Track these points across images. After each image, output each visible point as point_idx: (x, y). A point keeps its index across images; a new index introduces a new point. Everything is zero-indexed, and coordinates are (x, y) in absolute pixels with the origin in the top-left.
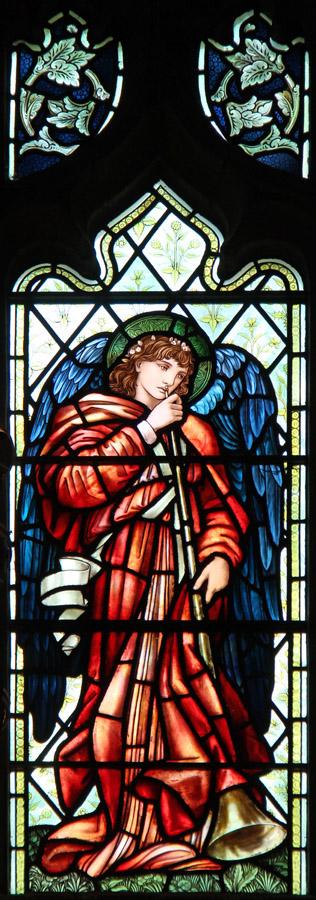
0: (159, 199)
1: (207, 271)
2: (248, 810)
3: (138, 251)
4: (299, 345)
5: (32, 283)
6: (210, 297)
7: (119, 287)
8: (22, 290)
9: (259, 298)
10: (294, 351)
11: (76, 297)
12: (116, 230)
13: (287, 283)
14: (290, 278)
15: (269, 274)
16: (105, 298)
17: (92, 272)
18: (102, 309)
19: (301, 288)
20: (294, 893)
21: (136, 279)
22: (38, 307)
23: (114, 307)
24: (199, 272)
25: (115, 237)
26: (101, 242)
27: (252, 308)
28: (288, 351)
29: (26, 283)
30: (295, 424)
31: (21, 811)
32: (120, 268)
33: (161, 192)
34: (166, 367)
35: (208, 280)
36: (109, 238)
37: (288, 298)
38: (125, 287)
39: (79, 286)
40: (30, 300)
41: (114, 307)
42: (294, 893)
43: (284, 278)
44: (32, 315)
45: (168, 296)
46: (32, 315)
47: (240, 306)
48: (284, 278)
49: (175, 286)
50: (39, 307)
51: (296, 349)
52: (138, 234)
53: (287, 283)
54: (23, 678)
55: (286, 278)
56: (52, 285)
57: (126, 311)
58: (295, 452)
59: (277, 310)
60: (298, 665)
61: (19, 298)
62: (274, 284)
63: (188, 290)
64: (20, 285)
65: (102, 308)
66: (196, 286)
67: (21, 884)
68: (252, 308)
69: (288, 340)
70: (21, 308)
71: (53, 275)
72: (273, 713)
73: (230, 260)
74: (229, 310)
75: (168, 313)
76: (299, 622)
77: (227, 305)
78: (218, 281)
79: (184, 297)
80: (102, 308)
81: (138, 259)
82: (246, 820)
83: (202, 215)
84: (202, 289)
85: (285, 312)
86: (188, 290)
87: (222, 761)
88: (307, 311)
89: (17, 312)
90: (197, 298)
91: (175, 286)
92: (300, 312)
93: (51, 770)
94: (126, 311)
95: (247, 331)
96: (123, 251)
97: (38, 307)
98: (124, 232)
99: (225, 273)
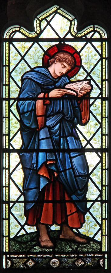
1: (72, 30)
3: (49, 23)
5: (11, 34)
6: (76, 39)
7: (43, 36)
8: (8, 37)
9: (90, 40)
11: (28, 40)
13: (100, 35)
15: (95, 31)
16: (37, 40)
17: (31, 29)
18: (36, 44)
20: (8, 43)
21: (48, 34)
22: (14, 43)
24: (70, 32)
25: (41, 21)
26: (36, 23)
28: (101, 59)
29: (9, 34)
31: (7, 123)
34: (65, 67)
35: (73, 33)
37: (101, 40)
39: (27, 34)
40: (11, 41)
42: (8, 43)
43: (99, 33)
44: (11, 45)
45: (59, 39)
46: (11, 45)
47: (32, 43)
48: (99, 33)
49: (62, 36)
50: (14, 43)
51: (104, 56)
52: (49, 19)
53: (100, 35)
54: (7, 153)
56: (18, 36)
59: (97, 44)
60: (105, 79)
61: (6, 40)
62: (97, 36)
63: (66, 38)
64: (6, 36)
65: (89, 43)
66: (69, 36)
67: (7, 248)
71: (19, 31)
76: (6, 42)
78: (76, 31)
79: (65, 39)
80: (89, 43)
84: (72, 37)
85: (100, 45)
86: (66, 38)
87: (62, 170)
88: (108, 44)
89: (6, 45)
91: (62, 36)
92: (105, 44)
93: (11, 200)
95: (87, 50)
97: (14, 43)
98: (45, 18)
99: (80, 29)
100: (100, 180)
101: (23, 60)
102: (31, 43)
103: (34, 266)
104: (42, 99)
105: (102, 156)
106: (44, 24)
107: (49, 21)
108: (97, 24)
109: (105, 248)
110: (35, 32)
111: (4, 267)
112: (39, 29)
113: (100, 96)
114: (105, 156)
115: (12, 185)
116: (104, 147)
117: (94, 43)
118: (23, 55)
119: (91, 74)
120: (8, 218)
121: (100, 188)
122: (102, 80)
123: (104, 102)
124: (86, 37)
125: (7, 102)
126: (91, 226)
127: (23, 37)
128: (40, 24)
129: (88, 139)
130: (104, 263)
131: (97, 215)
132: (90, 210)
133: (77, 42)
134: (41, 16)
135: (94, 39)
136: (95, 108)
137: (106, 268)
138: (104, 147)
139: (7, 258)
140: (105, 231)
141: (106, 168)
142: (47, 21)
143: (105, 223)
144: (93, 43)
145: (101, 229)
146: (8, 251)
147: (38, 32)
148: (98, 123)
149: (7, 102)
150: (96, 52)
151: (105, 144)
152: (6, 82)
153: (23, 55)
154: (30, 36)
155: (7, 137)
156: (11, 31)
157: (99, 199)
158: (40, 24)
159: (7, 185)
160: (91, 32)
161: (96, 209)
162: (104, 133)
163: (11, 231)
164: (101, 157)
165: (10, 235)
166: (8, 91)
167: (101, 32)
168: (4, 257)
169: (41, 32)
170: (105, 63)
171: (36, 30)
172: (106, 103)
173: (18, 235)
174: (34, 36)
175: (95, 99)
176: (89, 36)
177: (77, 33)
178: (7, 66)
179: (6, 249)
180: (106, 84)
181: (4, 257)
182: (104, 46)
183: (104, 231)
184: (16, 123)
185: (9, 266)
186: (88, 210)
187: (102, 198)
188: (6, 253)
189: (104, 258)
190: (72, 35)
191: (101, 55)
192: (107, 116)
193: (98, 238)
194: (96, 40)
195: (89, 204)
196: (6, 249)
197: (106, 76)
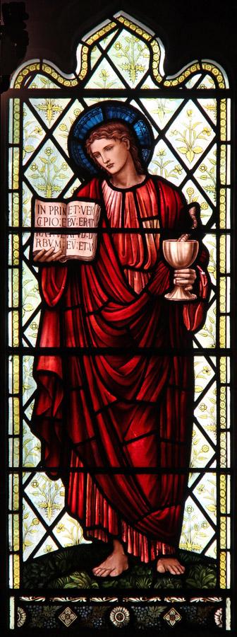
0: (120, 27)
2: (135, 175)
3: (104, 54)
4: (226, 134)
6: (163, 92)
8: (18, 86)
9: (196, 94)
10: (77, 83)
11: (62, 92)
12: (90, 42)
13: (216, 83)
14: (219, 78)
16: (78, 92)
17: (68, 65)
19: (228, 87)
21: (103, 79)
22: (31, 100)
23: (200, 100)
24: (150, 72)
25: (91, 48)
27: (190, 102)
28: (217, 140)
29: (21, 79)
30: (222, 200)
32: (149, 77)
33: (121, 20)
36: (86, 50)
37: (217, 94)
38: (98, 84)
39: (61, 80)
40: (26, 94)
41: (200, 100)
44: (25, 106)
46: (25, 106)
48: (214, 78)
50: (34, 101)
51: (223, 138)
52: (104, 44)
55: (212, 76)
56: (39, 82)
57: (90, 102)
58: (222, 226)
59: (209, 103)
60: (224, 548)
61: (15, 94)
62: (208, 83)
63: (142, 88)
64: (15, 83)
65: (77, 101)
66: (149, 84)
67: (17, 581)
68: (190, 102)
69: (217, 129)
70: (17, 101)
72: (195, 426)
73: (172, 66)
74: (174, 104)
75: (89, 603)
77: (168, 100)
79: (139, 93)
80: (77, 101)
81: (105, 59)
82: (136, 179)
83: (8, 390)
90: (150, 94)
91: (133, 86)
92: (227, 105)
93: (26, 465)
94: (90, 102)
96: (96, 54)
97: (31, 100)
98: (96, 43)
99: (171, 68)
100: (214, 502)
101: (49, 127)
102: (68, 100)
103: (74, 624)
104: (95, 232)
105: (220, 455)
106: (96, 54)
107: (104, 48)
108: (204, 58)
109: (226, 582)
110: (75, 74)
111: (12, 626)
112: (85, 65)
113: (214, 227)
114: (225, 362)
115: (27, 509)
116: (222, 346)
117: (203, 102)
118: (49, 128)
119: (194, 175)
120: (17, 188)
121: (215, 521)
122: (219, 186)
123: (222, 478)
124: (185, 88)
125: (16, 238)
126: (197, 135)
127: (52, 86)
128: (89, 55)
129: (190, 167)
130: (224, 618)
131: (209, 503)
132: (194, 175)
133: (163, 100)
134: (90, 38)
135: (200, 90)
136: (202, 174)
137: (228, 628)
138: (222, 346)
139: (19, 603)
140: (226, 540)
141: (226, 586)
142: (100, 48)
143: (226, 524)
144: (201, 101)
145: (217, 537)
146: (18, 588)
147: (84, 73)
148: (210, 368)
149: (16, 238)
150: (204, 519)
151: (225, 541)
152: (13, 261)
153: (49, 128)
154: (67, 84)
155: (17, 401)
156: (26, 72)
157: (214, 465)
158: (89, 55)
159: (17, 434)
160: (192, 75)
161: (206, 490)
162: (222, 310)
163: (26, 539)
164: (217, 369)
165: (23, 311)
166: (18, 376)
167: (215, 72)
168: (12, 600)
169: (90, 72)
170: (227, 151)
171: (78, 71)
172: (226, 481)
173: (36, 556)
174: (75, 83)
175: (202, 472)
176: (190, 85)
177: (164, 79)
178: (17, 436)
179: (14, 581)
180: (227, 194)
181: (12, 600)
182: (223, 154)
183: (222, 542)
184: (35, 484)
185: (22, 622)
186: (189, 492)
187: (218, 226)
188: (14, 592)
189: (223, 605)
190: (154, 79)
191: (217, 129)
192: (228, 382)
193: (212, 553)
194: (207, 94)
195: (192, 479)
196: (14, 581)
197: (226, 178)
